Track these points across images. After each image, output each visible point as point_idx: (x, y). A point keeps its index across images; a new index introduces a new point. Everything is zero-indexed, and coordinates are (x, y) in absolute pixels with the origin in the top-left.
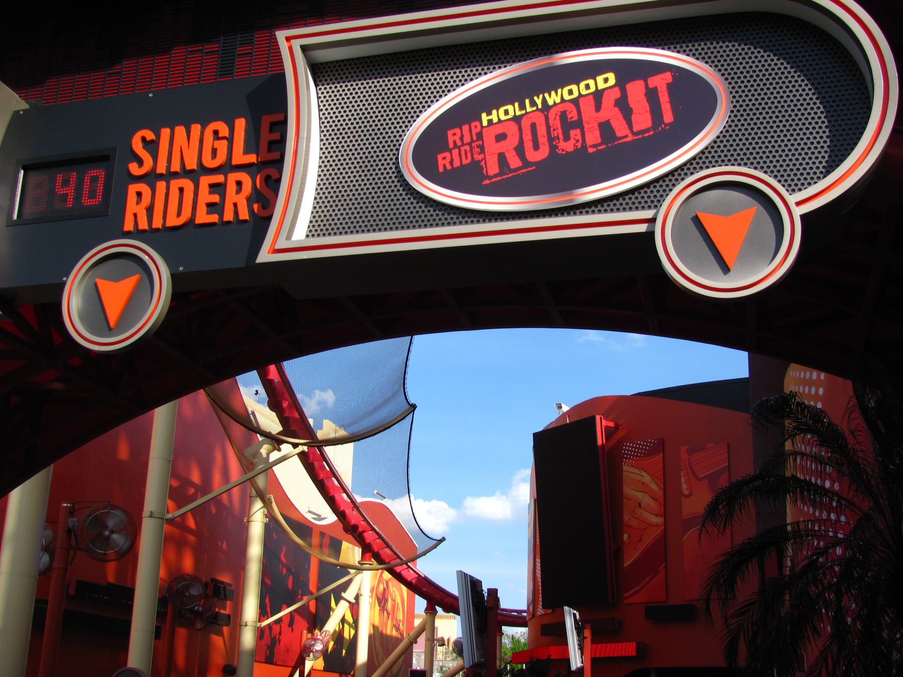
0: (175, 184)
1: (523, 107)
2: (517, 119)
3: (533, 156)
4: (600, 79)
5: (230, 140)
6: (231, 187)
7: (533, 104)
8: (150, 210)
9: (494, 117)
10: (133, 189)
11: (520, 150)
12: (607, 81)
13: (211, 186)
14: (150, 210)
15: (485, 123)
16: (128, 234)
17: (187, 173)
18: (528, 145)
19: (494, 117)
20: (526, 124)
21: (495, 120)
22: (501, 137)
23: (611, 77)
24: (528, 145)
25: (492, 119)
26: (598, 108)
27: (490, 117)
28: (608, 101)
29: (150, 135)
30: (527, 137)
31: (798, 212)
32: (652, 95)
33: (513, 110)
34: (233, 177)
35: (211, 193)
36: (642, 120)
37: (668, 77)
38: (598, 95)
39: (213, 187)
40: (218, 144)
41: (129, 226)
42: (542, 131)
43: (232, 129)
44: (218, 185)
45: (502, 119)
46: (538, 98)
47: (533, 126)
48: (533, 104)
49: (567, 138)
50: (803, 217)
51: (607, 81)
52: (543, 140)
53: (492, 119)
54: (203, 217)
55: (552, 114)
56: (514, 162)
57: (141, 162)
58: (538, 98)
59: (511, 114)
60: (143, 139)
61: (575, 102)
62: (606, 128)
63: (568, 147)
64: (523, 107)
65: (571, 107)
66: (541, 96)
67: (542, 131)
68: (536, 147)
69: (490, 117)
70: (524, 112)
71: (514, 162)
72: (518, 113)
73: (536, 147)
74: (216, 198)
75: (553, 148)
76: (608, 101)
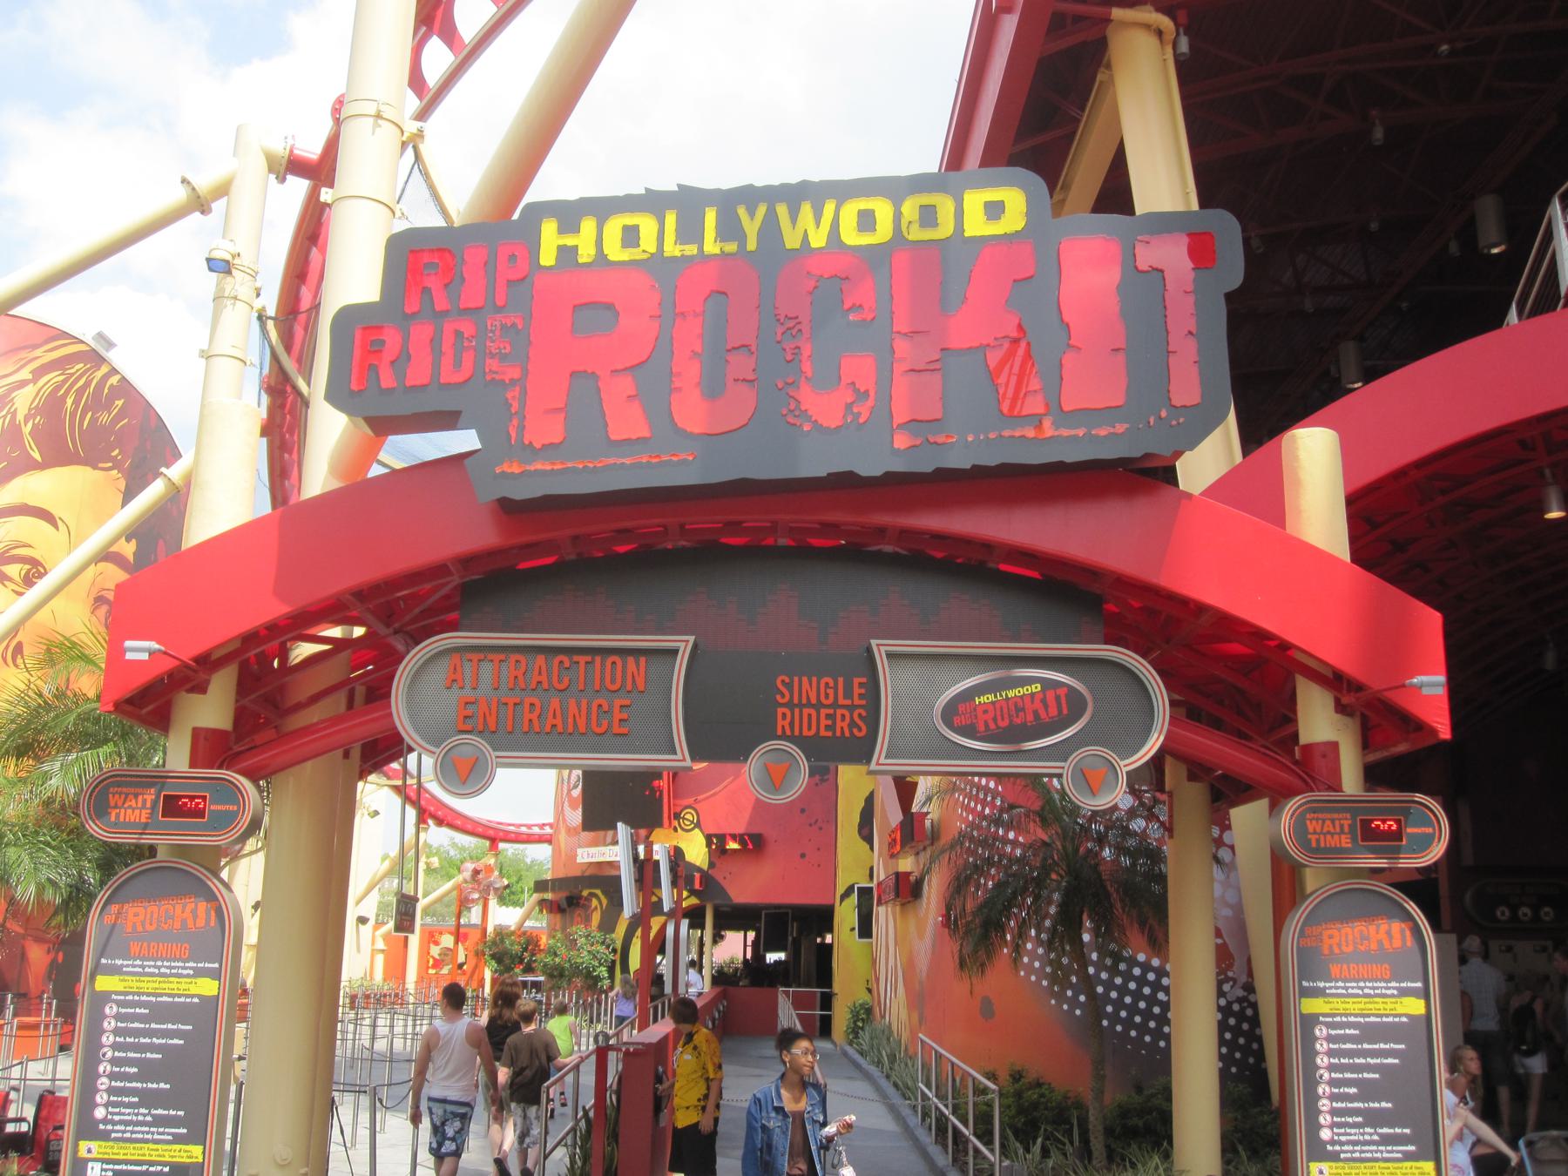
0: (806, 711)
1: (996, 696)
2: (993, 703)
3: (1001, 724)
4: (1033, 686)
5: (836, 688)
6: (839, 717)
7: (1001, 695)
8: (792, 724)
9: (982, 700)
10: (780, 710)
11: (995, 720)
12: (1037, 688)
13: (827, 715)
14: (792, 724)
15: (547, 258)
16: (779, 738)
17: (809, 704)
18: (999, 718)
19: (982, 700)
20: (997, 706)
21: (586, 254)
22: (985, 712)
23: (1039, 685)
24: (999, 718)
25: (575, 248)
26: (1032, 702)
27: (569, 241)
28: (1037, 701)
29: (787, 680)
30: (998, 713)
31: (1125, 770)
32: (1057, 698)
33: (991, 698)
34: (839, 712)
35: (826, 719)
36: (1053, 712)
37: (1065, 689)
38: (1032, 695)
39: (828, 716)
40: (829, 691)
41: (779, 732)
42: (1005, 711)
43: (836, 682)
44: (831, 715)
45: (612, 257)
46: (752, 215)
47: (1001, 708)
48: (1001, 695)
49: (1017, 716)
50: (1127, 773)
51: (1037, 688)
52: (1006, 716)
53: (575, 248)
54: (823, 733)
55: (1010, 702)
56: (992, 726)
57: (783, 695)
58: (752, 215)
59: (648, 244)
60: (783, 681)
61: (1021, 697)
62: (1036, 713)
63: (1018, 721)
64: (996, 696)
65: (1019, 700)
66: (762, 210)
67: (1005, 711)
68: (1003, 719)
69: (569, 241)
70: (691, 250)
71: (992, 726)
72: (672, 249)
73: (1003, 719)
74: (830, 722)
75: (1011, 721)
76: (1037, 701)
